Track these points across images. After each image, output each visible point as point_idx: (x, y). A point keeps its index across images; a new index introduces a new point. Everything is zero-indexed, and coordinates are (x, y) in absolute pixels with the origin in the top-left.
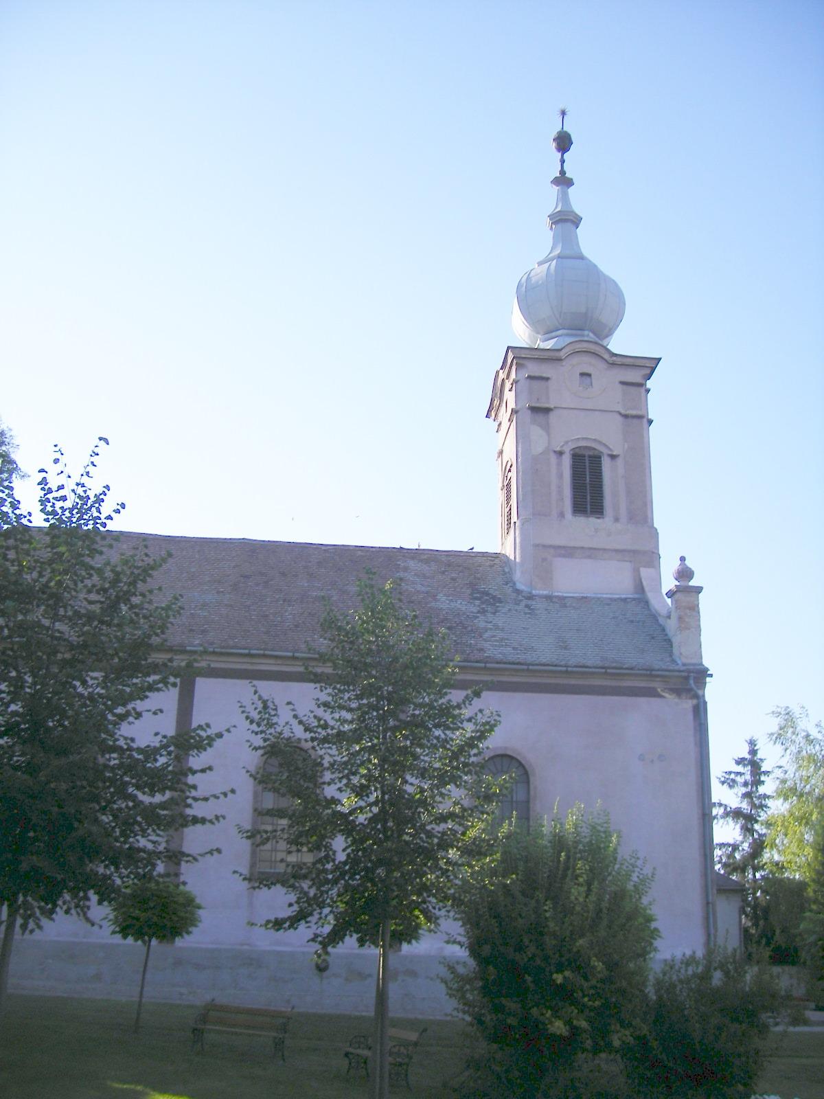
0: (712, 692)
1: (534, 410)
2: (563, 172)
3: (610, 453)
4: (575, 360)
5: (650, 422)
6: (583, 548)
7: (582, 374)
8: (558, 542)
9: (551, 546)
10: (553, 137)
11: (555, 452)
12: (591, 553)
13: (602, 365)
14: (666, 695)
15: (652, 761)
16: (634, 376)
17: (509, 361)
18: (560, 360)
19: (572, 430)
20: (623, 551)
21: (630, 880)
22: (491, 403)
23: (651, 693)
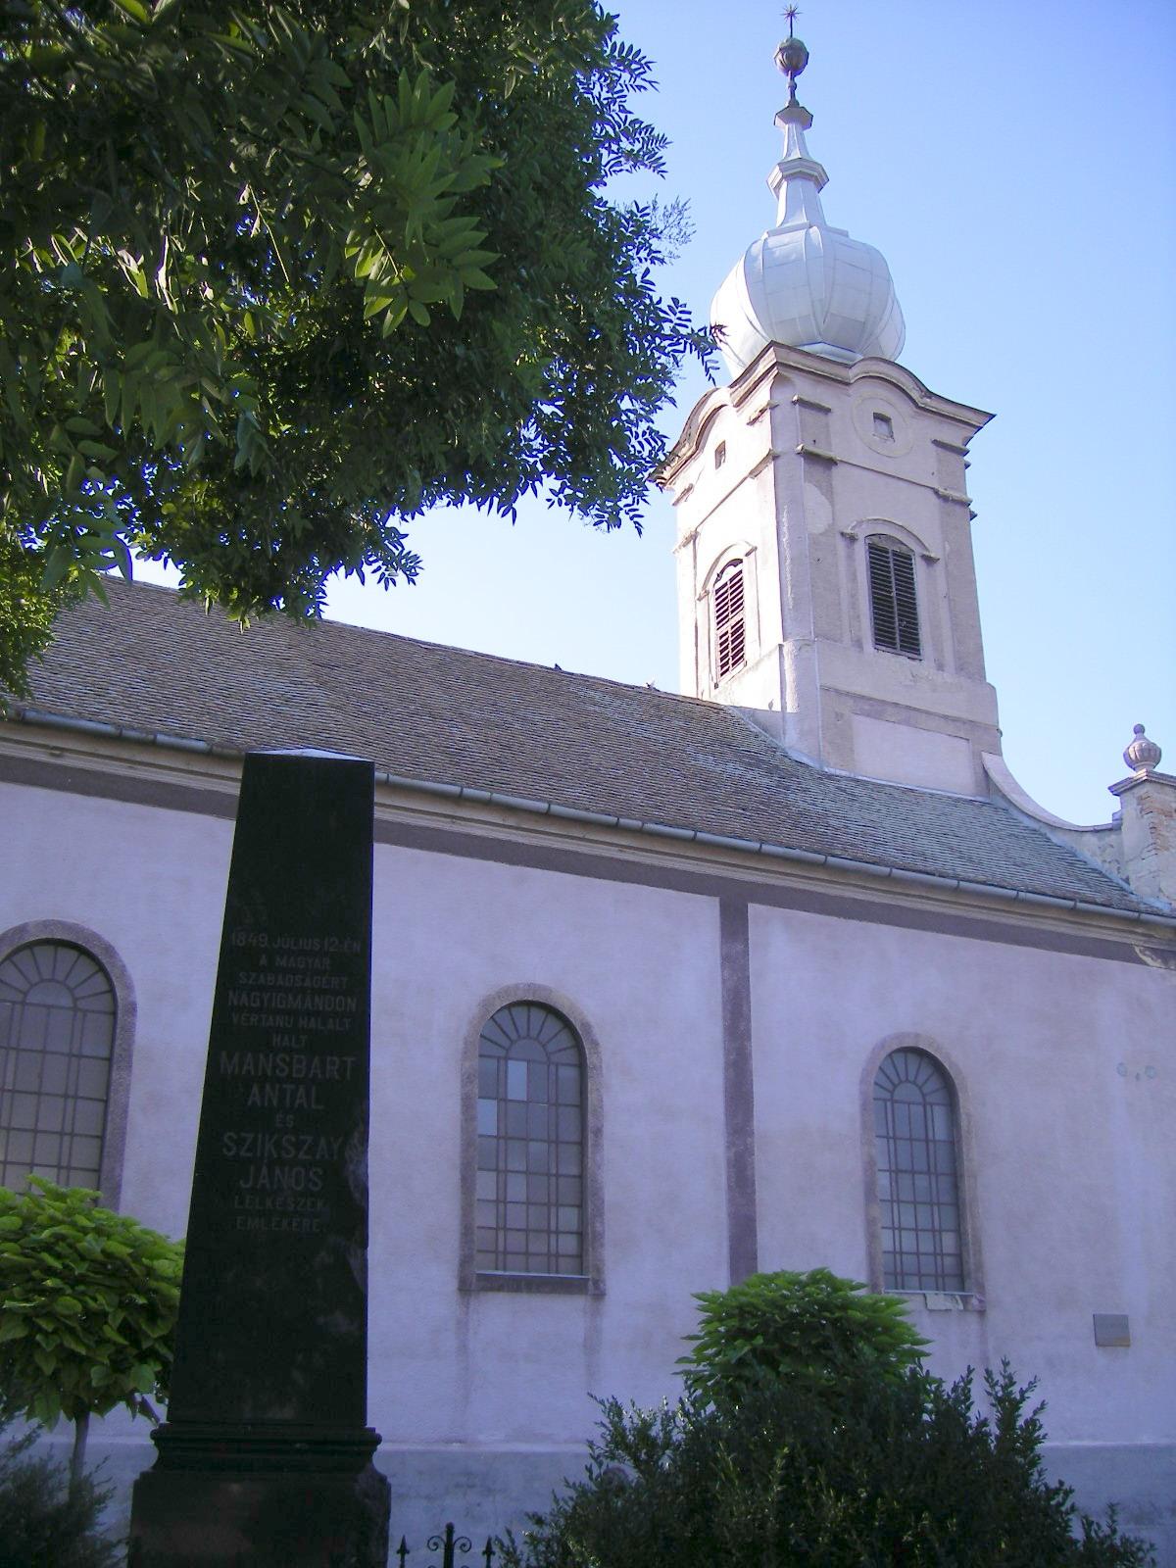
1: (810, 457)
2: (794, 103)
3: (926, 553)
5: (973, 516)
6: (896, 704)
7: (878, 417)
8: (857, 689)
9: (848, 694)
11: (842, 534)
12: (909, 715)
13: (906, 408)
14: (1148, 960)
15: (1138, 1077)
16: (951, 435)
17: (761, 369)
18: (848, 384)
19: (875, 504)
20: (955, 720)
21: (80, 1413)
23: (1127, 955)
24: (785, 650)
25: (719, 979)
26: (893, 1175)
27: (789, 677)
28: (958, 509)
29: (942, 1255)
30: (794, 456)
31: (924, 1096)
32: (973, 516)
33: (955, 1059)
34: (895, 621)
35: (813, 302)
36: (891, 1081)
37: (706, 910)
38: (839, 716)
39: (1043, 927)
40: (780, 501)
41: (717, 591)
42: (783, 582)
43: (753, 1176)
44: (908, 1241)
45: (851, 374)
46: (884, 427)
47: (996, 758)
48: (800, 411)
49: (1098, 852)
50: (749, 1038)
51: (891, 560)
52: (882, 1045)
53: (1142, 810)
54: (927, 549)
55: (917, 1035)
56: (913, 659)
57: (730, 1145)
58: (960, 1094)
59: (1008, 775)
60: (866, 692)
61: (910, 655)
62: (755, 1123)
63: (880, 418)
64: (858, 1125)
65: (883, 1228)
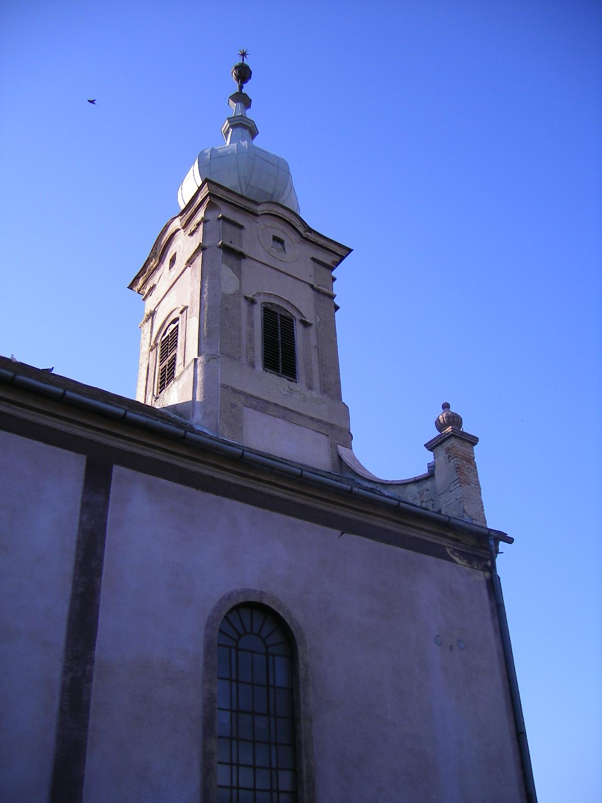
0: (506, 562)
1: (226, 249)
4: (270, 222)
5: (337, 308)
6: (276, 405)
8: (249, 391)
9: (241, 393)
10: (235, 65)
11: (246, 298)
12: (286, 414)
13: (295, 237)
14: (457, 559)
15: (451, 648)
17: (199, 199)
18: (256, 215)
19: (263, 284)
22: (145, 266)
23: (439, 553)
24: (199, 361)
25: (77, 522)
26: (234, 714)
27: (200, 378)
28: (327, 299)
29: (279, 792)
30: (217, 249)
31: (267, 647)
32: (337, 308)
33: (297, 615)
34: (279, 354)
35: (239, 177)
36: (236, 631)
37: (72, 467)
38: (234, 406)
39: (375, 523)
40: (205, 274)
41: (162, 342)
42: (202, 321)
43: (89, 701)
44: (246, 778)
45: (260, 209)
46: (280, 246)
47: (347, 450)
48: (223, 223)
49: (418, 496)
50: (100, 575)
51: (279, 319)
52: (229, 597)
53: (449, 457)
54: (304, 318)
55: (262, 593)
56: (291, 381)
57: (67, 670)
58: (299, 647)
59: (355, 459)
60: (255, 393)
61: (289, 378)
62: (97, 653)
63: (276, 239)
64: (201, 664)
65: (219, 763)
